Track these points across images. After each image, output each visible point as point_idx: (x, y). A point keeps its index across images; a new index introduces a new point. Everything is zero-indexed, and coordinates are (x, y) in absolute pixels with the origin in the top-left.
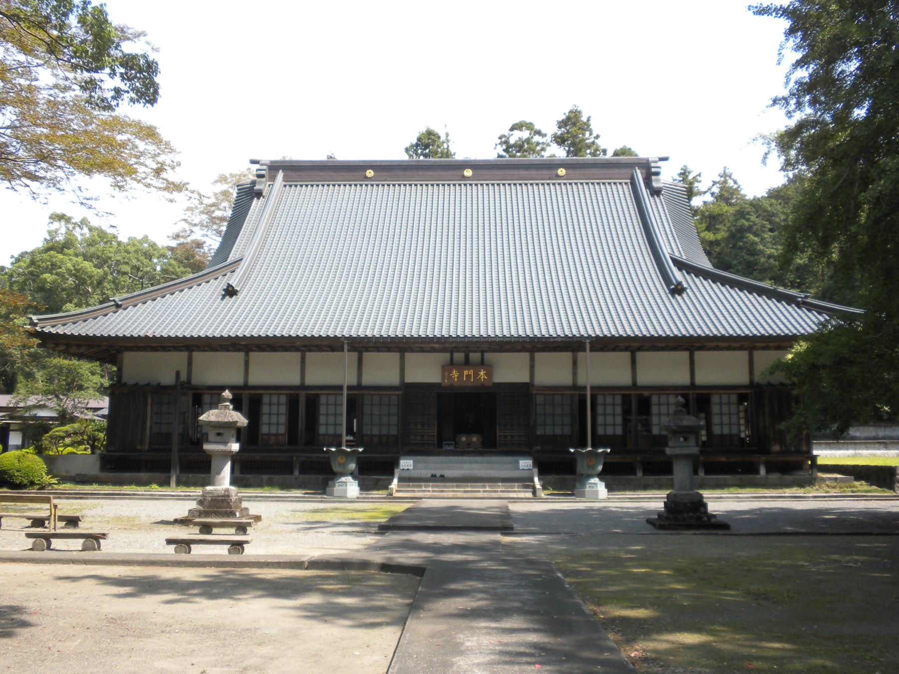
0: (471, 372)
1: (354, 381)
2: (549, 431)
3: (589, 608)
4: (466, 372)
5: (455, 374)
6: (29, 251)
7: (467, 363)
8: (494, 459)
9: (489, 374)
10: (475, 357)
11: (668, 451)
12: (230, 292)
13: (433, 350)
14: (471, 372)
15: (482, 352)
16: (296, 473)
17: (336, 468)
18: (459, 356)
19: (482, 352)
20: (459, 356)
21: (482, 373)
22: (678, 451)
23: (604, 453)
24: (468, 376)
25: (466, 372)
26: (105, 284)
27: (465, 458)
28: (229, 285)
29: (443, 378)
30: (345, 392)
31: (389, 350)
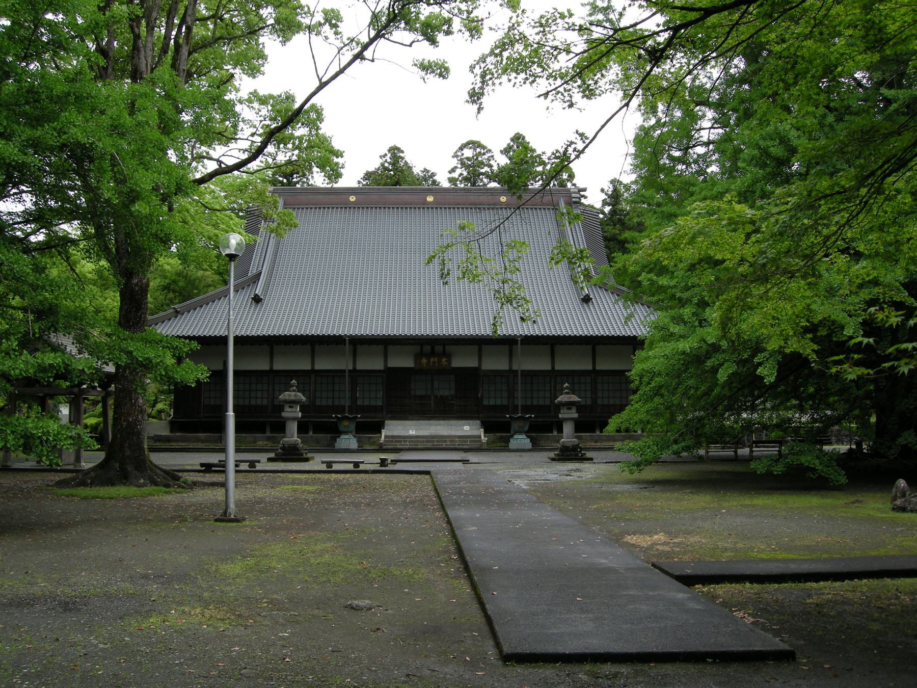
0: (436, 359)
1: (351, 367)
2: (492, 402)
3: (127, 445)
4: (432, 359)
5: (424, 361)
6: (275, 93)
7: (433, 353)
8: (453, 422)
9: (449, 361)
10: (439, 348)
11: (560, 416)
12: (257, 300)
13: (411, 344)
14: (436, 359)
15: (444, 345)
16: (311, 433)
17: (341, 428)
18: (427, 348)
19: (444, 345)
20: (427, 348)
21: (444, 360)
22: (566, 416)
23: (530, 417)
24: (434, 362)
25: (432, 359)
26: (579, 45)
27: (432, 422)
28: (256, 295)
29: (415, 363)
30: (347, 374)
31: (378, 344)
